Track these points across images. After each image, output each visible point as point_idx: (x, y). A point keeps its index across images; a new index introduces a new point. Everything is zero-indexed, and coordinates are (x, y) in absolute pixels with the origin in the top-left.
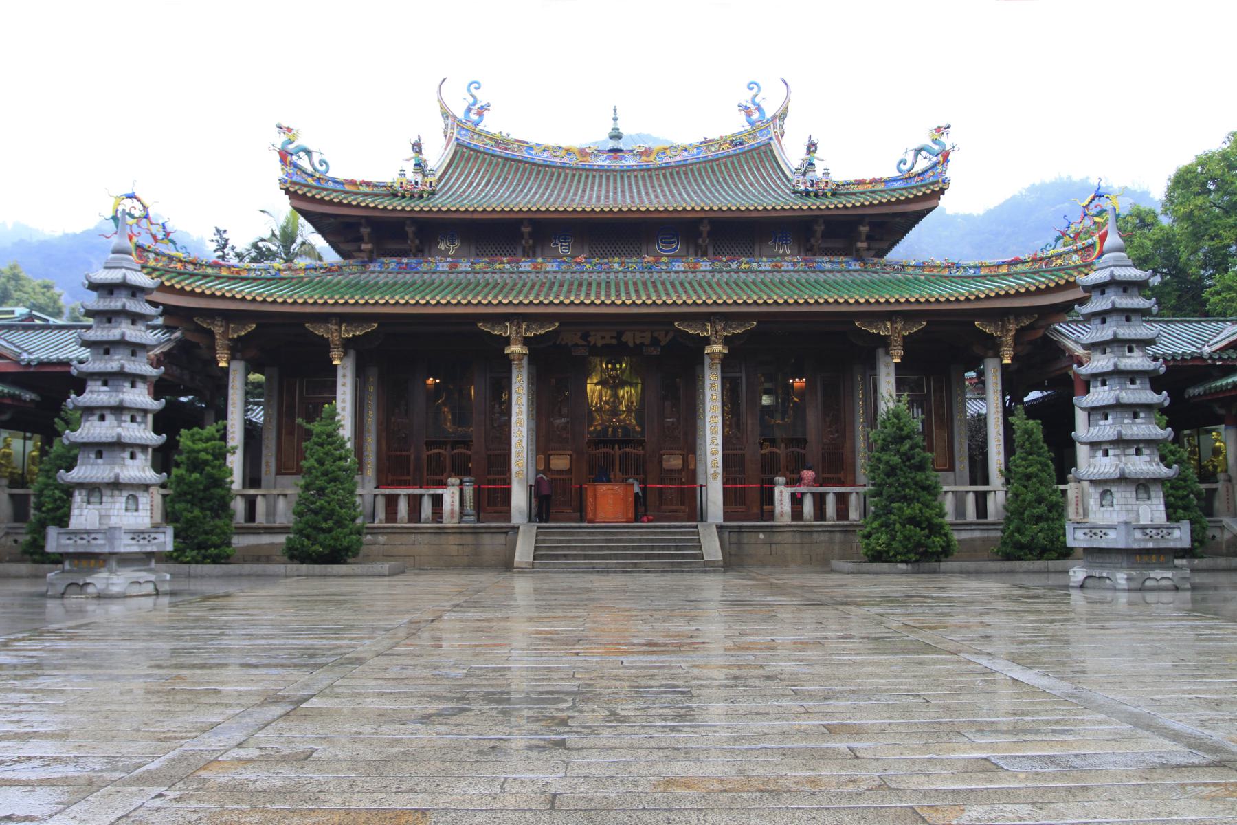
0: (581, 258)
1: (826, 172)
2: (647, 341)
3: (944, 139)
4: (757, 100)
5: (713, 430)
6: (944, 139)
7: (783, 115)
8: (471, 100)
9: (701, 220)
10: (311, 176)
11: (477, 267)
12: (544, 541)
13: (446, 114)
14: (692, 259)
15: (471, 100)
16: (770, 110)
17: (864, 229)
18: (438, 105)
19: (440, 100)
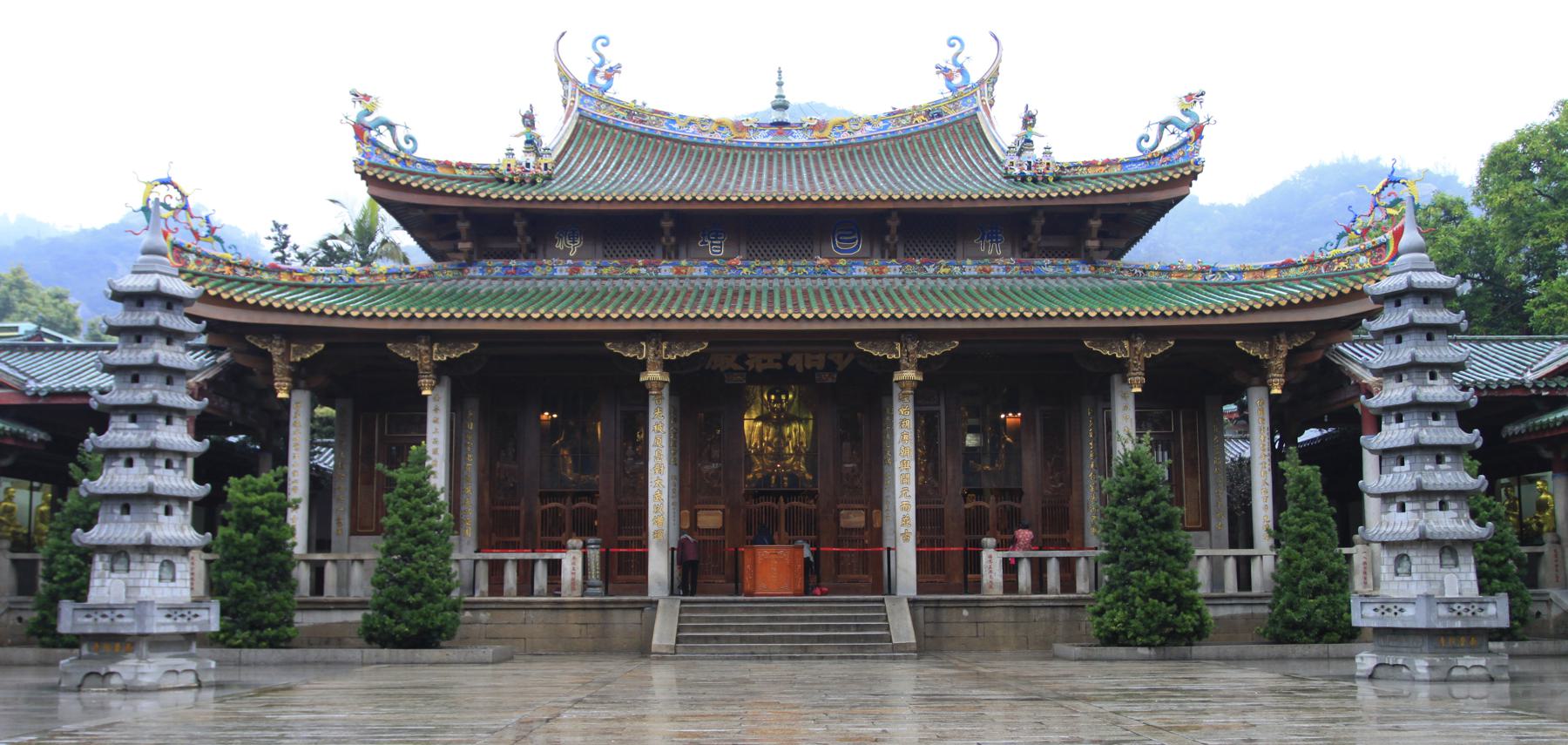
0: (737, 261)
2: (820, 366)
3: (1196, 109)
4: (960, 60)
5: (904, 478)
6: (1196, 109)
7: (992, 79)
8: (597, 60)
9: (886, 213)
10: (395, 156)
11: (605, 271)
12: (689, 619)
13: (565, 78)
14: (877, 262)
15: (597, 60)
18: (555, 66)
19: (558, 59)
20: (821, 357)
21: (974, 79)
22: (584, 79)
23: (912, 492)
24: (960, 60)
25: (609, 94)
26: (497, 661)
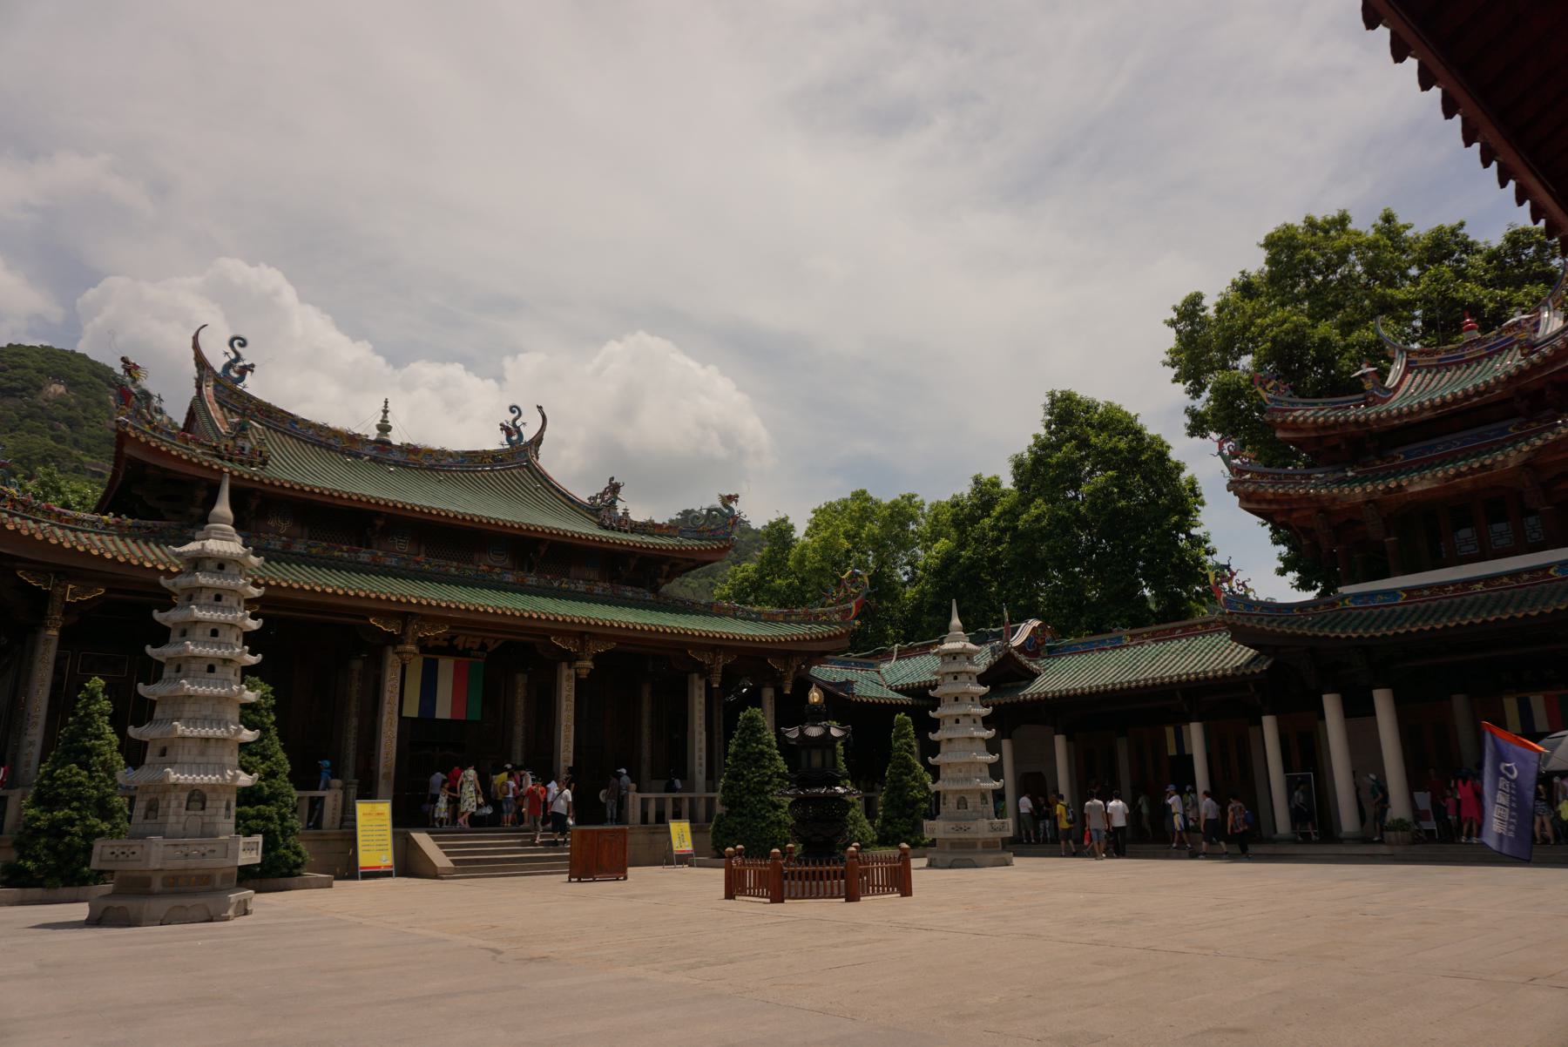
0: (421, 558)
1: (626, 513)
2: (476, 647)
3: (733, 505)
4: (518, 423)
5: (567, 737)
6: (733, 505)
7: (538, 440)
8: (233, 356)
9: (378, 514)
10: (149, 423)
11: (314, 551)
12: (1372, 796)
13: (201, 362)
14: (522, 574)
15: (233, 356)
16: (528, 434)
17: (380, 523)
18: (192, 354)
19: (196, 346)
20: (479, 641)
21: (527, 438)
22: (219, 369)
23: (571, 748)
24: (518, 423)
25: (240, 386)
26: (94, 922)
